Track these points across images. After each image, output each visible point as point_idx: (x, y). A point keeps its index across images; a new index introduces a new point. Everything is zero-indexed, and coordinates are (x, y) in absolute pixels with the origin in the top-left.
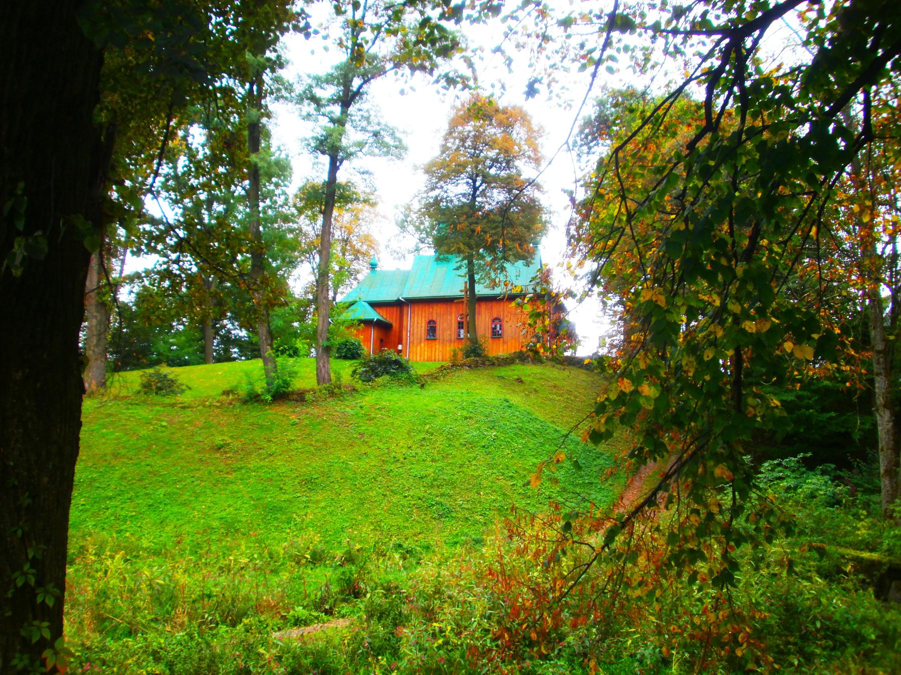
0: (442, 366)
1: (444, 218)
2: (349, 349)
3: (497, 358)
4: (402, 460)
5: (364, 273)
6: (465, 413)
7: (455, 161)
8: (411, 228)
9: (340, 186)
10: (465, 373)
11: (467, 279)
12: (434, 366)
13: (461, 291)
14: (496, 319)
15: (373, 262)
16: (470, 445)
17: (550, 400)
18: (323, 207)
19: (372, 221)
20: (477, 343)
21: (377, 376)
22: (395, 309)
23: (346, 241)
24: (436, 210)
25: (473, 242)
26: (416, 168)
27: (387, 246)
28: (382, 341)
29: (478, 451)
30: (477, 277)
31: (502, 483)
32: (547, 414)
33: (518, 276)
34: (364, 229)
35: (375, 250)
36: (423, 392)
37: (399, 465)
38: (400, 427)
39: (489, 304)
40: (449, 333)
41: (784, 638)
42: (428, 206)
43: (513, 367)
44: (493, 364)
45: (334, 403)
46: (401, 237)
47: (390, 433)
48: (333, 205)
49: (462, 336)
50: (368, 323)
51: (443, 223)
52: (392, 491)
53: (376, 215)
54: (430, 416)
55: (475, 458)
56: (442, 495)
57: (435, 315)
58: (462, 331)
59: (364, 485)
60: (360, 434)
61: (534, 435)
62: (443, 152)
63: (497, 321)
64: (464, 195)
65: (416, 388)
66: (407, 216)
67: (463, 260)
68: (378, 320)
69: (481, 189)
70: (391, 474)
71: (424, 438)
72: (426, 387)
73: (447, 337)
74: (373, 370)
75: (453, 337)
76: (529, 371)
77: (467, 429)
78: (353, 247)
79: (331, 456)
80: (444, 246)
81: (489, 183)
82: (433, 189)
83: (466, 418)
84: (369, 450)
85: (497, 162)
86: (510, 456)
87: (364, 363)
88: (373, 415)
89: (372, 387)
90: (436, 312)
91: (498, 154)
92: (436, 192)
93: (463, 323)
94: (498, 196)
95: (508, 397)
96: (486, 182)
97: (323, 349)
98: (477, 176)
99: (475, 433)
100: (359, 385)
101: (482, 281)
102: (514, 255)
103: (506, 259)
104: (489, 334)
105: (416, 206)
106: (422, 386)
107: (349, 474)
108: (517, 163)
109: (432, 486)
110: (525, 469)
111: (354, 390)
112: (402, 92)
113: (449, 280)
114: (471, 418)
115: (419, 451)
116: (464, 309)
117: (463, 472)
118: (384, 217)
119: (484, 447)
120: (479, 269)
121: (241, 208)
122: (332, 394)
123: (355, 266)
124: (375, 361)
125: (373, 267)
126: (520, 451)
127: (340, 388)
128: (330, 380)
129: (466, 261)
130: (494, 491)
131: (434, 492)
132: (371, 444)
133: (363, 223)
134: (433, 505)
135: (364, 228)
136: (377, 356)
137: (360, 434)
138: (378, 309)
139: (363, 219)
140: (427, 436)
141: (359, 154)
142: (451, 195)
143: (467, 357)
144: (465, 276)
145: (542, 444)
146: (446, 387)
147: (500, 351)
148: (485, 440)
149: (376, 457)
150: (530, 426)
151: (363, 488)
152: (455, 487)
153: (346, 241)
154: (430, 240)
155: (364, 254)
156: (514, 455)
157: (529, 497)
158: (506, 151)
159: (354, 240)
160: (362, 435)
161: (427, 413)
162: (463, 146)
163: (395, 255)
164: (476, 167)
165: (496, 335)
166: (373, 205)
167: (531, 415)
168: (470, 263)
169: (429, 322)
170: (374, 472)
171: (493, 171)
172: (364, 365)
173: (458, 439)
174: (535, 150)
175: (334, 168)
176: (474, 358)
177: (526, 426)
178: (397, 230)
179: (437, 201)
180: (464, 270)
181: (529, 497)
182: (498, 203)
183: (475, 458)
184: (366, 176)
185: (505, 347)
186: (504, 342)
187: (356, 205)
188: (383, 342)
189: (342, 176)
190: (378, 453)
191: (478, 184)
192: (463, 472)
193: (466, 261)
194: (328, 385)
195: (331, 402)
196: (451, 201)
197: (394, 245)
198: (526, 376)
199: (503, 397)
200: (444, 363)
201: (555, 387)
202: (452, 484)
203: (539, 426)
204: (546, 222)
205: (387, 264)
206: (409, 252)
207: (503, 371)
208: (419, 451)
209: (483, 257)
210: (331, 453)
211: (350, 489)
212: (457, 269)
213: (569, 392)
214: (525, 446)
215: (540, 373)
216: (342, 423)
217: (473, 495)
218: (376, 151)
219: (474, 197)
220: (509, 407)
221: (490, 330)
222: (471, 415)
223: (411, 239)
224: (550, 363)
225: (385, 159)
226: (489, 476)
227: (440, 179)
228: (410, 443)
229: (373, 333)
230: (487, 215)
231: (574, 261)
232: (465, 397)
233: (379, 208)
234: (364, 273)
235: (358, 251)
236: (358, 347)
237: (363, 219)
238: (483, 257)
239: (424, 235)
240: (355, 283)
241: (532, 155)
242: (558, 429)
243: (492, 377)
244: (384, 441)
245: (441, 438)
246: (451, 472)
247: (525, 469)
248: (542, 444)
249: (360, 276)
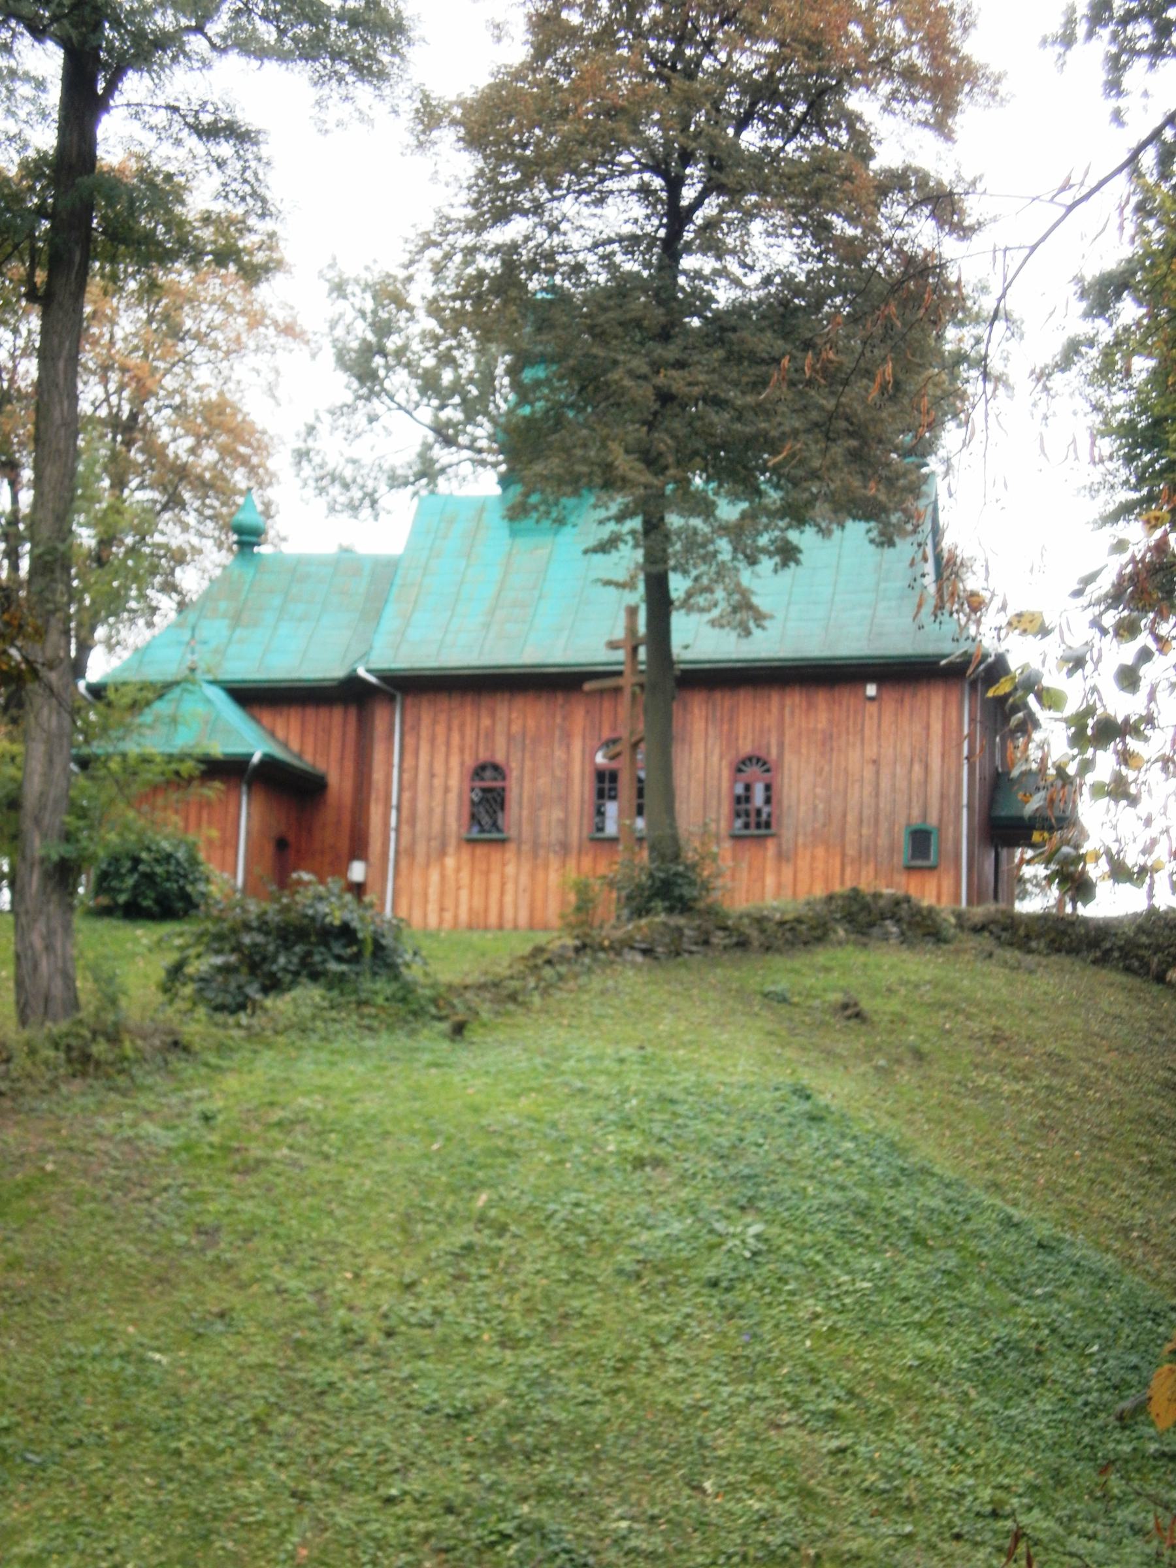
0: (538, 950)
1: (548, 344)
2: (149, 878)
3: (760, 921)
4: (376, 1338)
5: (205, 567)
6: (633, 1143)
7: (596, 91)
8: (399, 381)
9: (111, 185)
10: (630, 978)
11: (637, 596)
12: (502, 953)
13: (613, 645)
14: (749, 760)
15: (246, 518)
16: (658, 1274)
17: (978, 1092)
18: (40, 276)
19: (236, 348)
20: (676, 857)
21: (273, 985)
22: (337, 713)
23: (129, 428)
24: (502, 305)
25: (663, 442)
26: (430, 116)
27: (302, 455)
28: (281, 845)
29: (688, 1303)
30: (678, 585)
31: (792, 1441)
32: (966, 1152)
33: (823, 593)
34: (205, 378)
35: (252, 470)
36: (463, 1054)
37: (363, 1361)
38: (370, 1199)
39: (723, 700)
40: (557, 814)
42: (472, 289)
43: (821, 956)
44: (743, 944)
45: (90, 1102)
46: (360, 419)
47: (327, 1224)
48: (83, 273)
49: (611, 829)
50: (227, 770)
51: (543, 359)
52: (333, 1478)
53: (256, 320)
54: (491, 1152)
55: (678, 1334)
56: (544, 1492)
57: (501, 741)
58: (611, 808)
59: (212, 1453)
60: (200, 1230)
61: (918, 1239)
62: (542, 52)
63: (753, 770)
64: (631, 243)
65: (432, 1039)
66: (383, 329)
67: (620, 518)
68: (269, 762)
69: (699, 217)
70: (330, 1401)
71: (469, 1248)
72: (474, 1033)
73: (550, 832)
74: (255, 962)
75: (578, 831)
76: (888, 971)
77: (643, 1207)
78: (155, 452)
79: (74, 1330)
80: (543, 463)
81: (734, 193)
82: (502, 215)
83: (639, 1163)
84: (236, 1300)
85: (774, 97)
86: (822, 1325)
87: (220, 937)
88: (256, 1151)
89: (252, 1035)
90: (507, 727)
91: (775, 60)
92: (517, 228)
93: (614, 777)
94: (769, 253)
95: (806, 1077)
96: (721, 189)
97: (47, 876)
98: (686, 158)
99: (676, 1227)
100: (197, 1026)
101: (701, 600)
102: (831, 498)
103: (797, 514)
104: (721, 818)
105: (422, 289)
106: (459, 1029)
107: (149, 1406)
108: (855, 100)
109: (502, 1453)
110: (887, 1384)
111: (177, 1045)
113: (564, 597)
114: (657, 1162)
115: (447, 1300)
116: (623, 719)
117: (630, 1391)
118: (289, 330)
119: (714, 1284)
120: (689, 549)
122: (82, 1062)
123: (169, 533)
124: (263, 927)
125: (247, 538)
126: (864, 1305)
127: (114, 1038)
128: (74, 1004)
129: (636, 523)
130: (761, 1477)
131: (511, 1480)
132: (246, 1271)
133: (199, 355)
134: (505, 1537)
135: (203, 375)
136: (271, 908)
137: (200, 1230)
138: (267, 717)
139: (200, 338)
140: (482, 1238)
141: (196, 43)
142: (576, 240)
143: (641, 912)
144: (629, 585)
145: (955, 1280)
146: (554, 1035)
147: (757, 886)
148: (718, 1257)
149: (265, 1327)
150: (906, 1202)
151: (209, 1468)
152: (597, 1459)
153: (129, 428)
154: (482, 431)
155: (203, 486)
156: (842, 1321)
157: (908, 1508)
158: (814, 48)
159: (160, 420)
160: (209, 1233)
161: (480, 1144)
162: (631, 23)
163: (335, 490)
164: (685, 121)
165: (754, 821)
166: (252, 274)
167: (904, 1153)
168: (653, 528)
169: (480, 771)
170: (260, 1391)
171: (752, 138)
172: (218, 941)
173: (608, 1251)
174: (937, 42)
175: (82, 103)
176: (668, 913)
177: (888, 1198)
178: (340, 386)
179: (508, 282)
180: (629, 557)
181: (908, 1508)
182: (767, 281)
183: (678, 1334)
184: (225, 149)
185: (787, 871)
186: (781, 857)
187: (181, 275)
188: (284, 853)
189: (117, 140)
190: (276, 1310)
191: (688, 194)
192: (630, 1391)
193: (636, 523)
194: (63, 1026)
195: (78, 1095)
196: (578, 269)
197: (332, 449)
198: (875, 993)
199: (784, 1077)
200: (541, 938)
201: (996, 1039)
202: (586, 1444)
203: (936, 1202)
204: (961, 358)
205: (302, 526)
206: (396, 481)
207: (785, 973)
208: (447, 1300)
209: (706, 508)
210: (73, 1317)
211: (153, 1471)
212: (606, 547)
213: (1058, 1064)
214: (885, 1284)
215: (935, 983)
216: (123, 1186)
217: (670, 1493)
218: (267, 32)
219: (672, 248)
220: (815, 1119)
221: (726, 808)
222: (661, 1150)
223: (401, 429)
224: (972, 942)
225: (299, 74)
226: (742, 1409)
227: (530, 170)
228: (410, 1267)
229: (247, 815)
230: (724, 327)
232: (634, 1081)
233: (267, 292)
234: (205, 567)
235: (182, 472)
236: (189, 870)
237: (200, 338)
238: (706, 508)
239: (452, 413)
240: (167, 604)
241: (922, 63)
242: (1017, 1214)
243: (742, 994)
244: (303, 1258)
245: (537, 1246)
246: (578, 1390)
247: (887, 1384)
248: (955, 1280)
249: (189, 579)
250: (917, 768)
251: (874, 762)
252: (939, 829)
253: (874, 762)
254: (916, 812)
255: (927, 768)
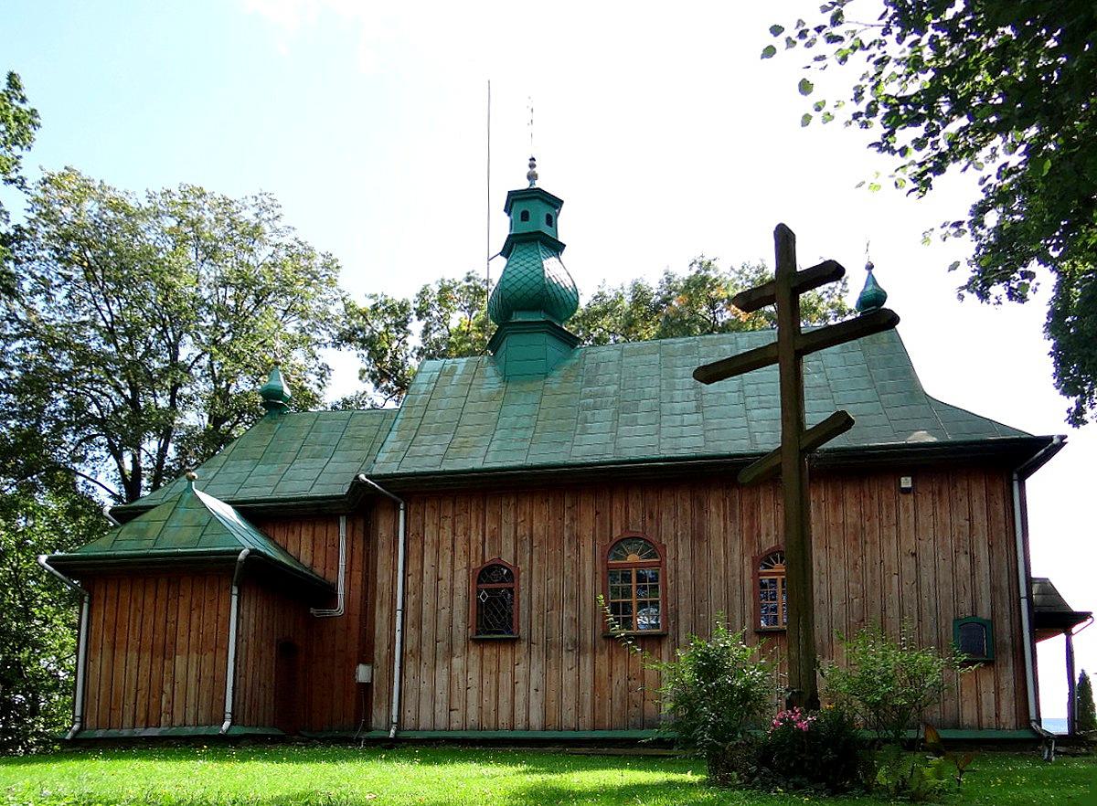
40: (568, 612)
41: (365, 323)
90: (507, 535)
112: (806, 120)
121: (53, 506)
231: (885, 122)
250: (964, 561)
251: (914, 555)
252: (992, 622)
253: (914, 555)
254: (966, 606)
255: (972, 558)
